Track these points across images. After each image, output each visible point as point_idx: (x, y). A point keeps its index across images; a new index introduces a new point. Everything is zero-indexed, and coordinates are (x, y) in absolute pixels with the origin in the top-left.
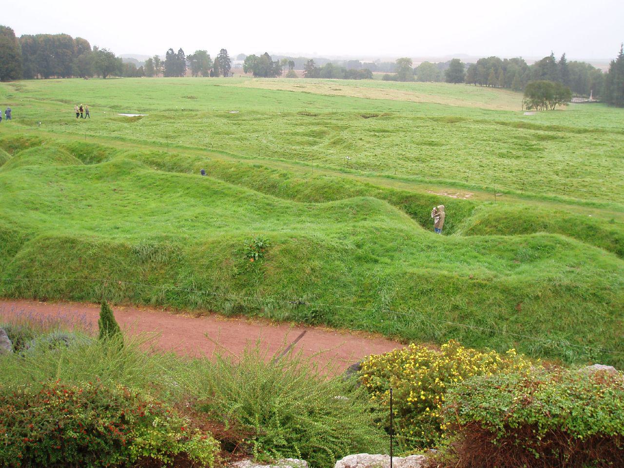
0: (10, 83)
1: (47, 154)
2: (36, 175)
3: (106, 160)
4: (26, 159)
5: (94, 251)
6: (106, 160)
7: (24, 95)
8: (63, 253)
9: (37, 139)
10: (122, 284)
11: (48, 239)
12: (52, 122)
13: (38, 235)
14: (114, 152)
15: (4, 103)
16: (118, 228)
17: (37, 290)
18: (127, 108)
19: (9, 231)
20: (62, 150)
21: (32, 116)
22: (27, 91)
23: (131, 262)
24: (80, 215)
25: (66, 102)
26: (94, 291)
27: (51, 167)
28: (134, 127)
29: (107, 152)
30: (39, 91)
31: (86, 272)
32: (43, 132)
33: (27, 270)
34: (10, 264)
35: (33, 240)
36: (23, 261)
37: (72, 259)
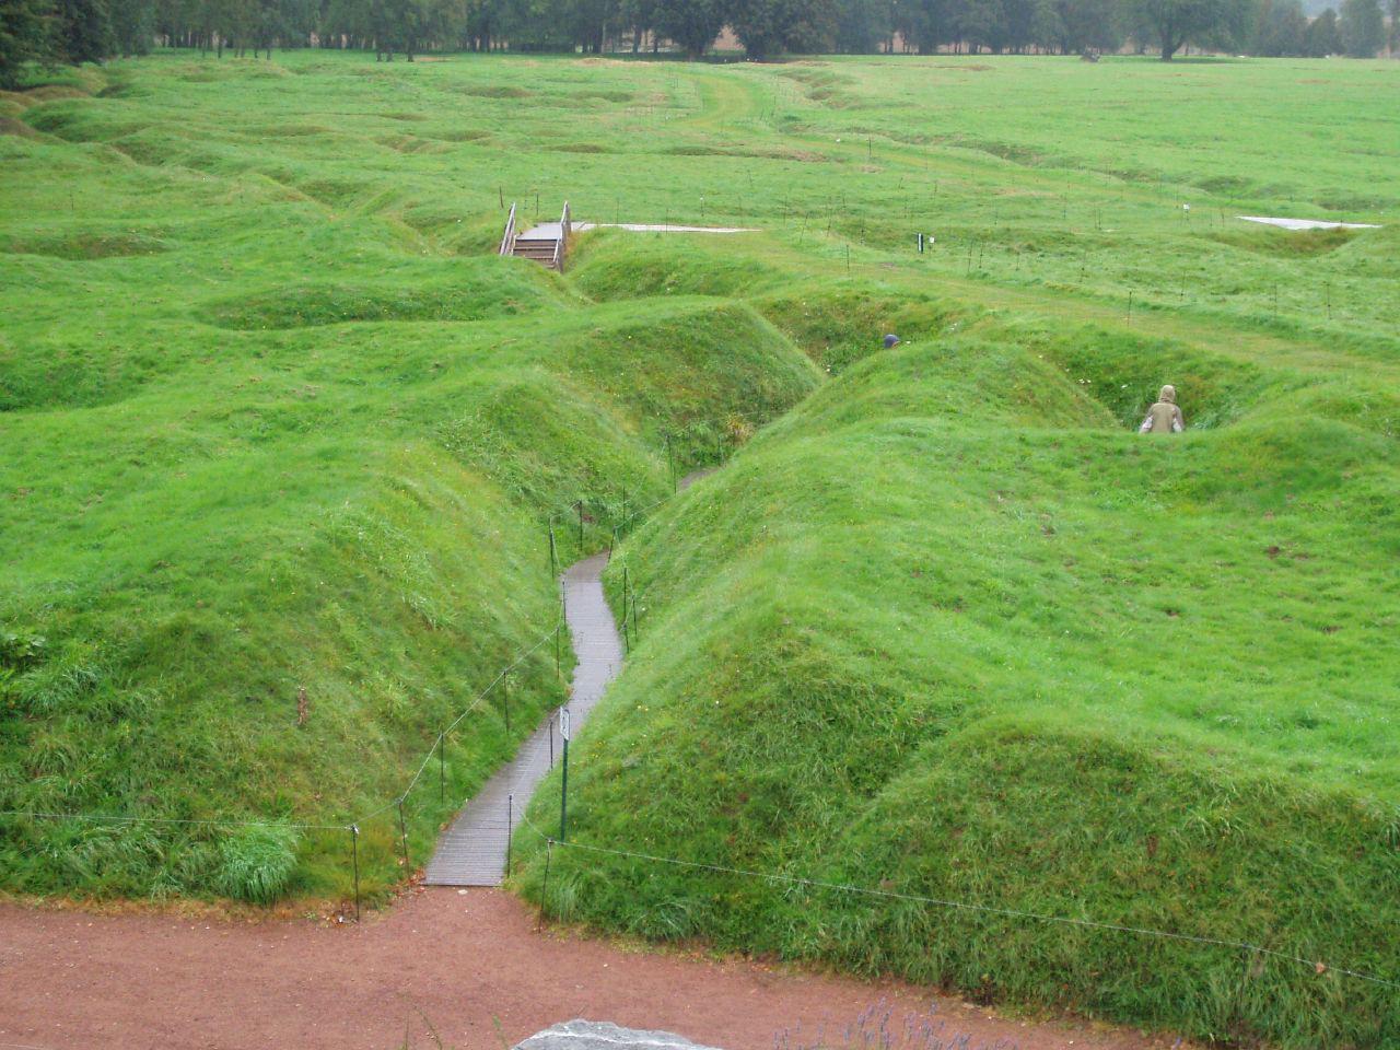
0: (787, 66)
1: (977, 373)
2: (939, 457)
3: (1211, 416)
4: (895, 391)
5: (1217, 815)
6: (1211, 416)
7: (844, 119)
8: (1079, 807)
9: (925, 308)
10: (1331, 978)
11: (1021, 738)
12: (979, 239)
13: (976, 716)
14: (1250, 384)
15: (769, 148)
16: (1310, 724)
17: (961, 949)
18: (1273, 190)
19: (858, 685)
20: (1038, 359)
21: (881, 210)
22: (858, 105)
23: (1374, 883)
24: (1136, 646)
25: (1013, 154)
26: (1204, 988)
27: (999, 432)
28: (1323, 277)
29: (1222, 381)
30: (903, 105)
31: (1174, 901)
32: (945, 277)
33: (923, 862)
34: (855, 824)
35: (955, 736)
36: (910, 822)
37: (1118, 839)
